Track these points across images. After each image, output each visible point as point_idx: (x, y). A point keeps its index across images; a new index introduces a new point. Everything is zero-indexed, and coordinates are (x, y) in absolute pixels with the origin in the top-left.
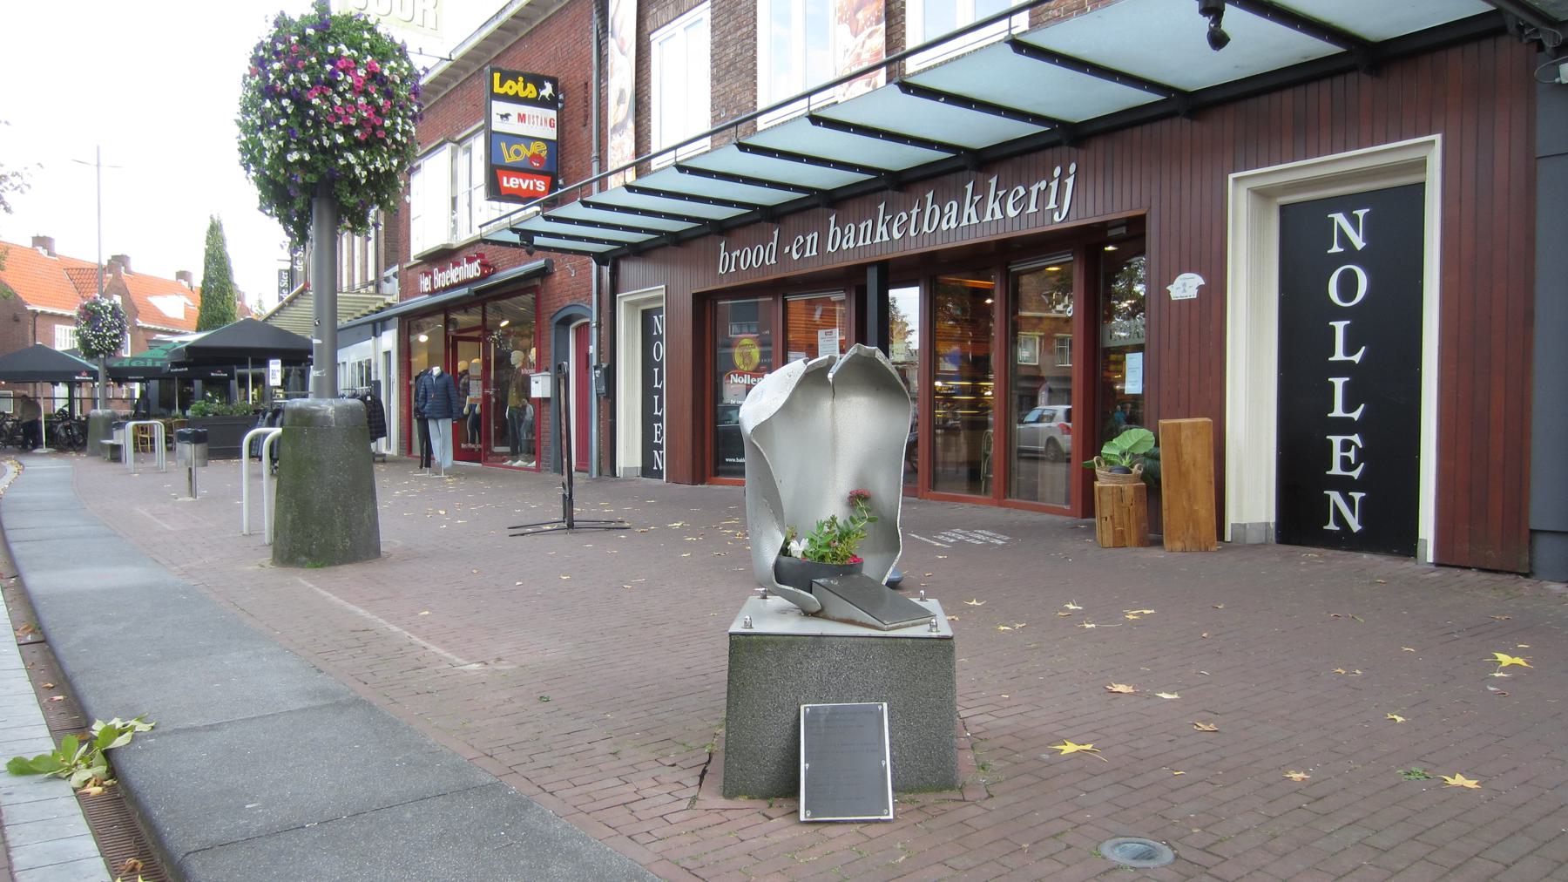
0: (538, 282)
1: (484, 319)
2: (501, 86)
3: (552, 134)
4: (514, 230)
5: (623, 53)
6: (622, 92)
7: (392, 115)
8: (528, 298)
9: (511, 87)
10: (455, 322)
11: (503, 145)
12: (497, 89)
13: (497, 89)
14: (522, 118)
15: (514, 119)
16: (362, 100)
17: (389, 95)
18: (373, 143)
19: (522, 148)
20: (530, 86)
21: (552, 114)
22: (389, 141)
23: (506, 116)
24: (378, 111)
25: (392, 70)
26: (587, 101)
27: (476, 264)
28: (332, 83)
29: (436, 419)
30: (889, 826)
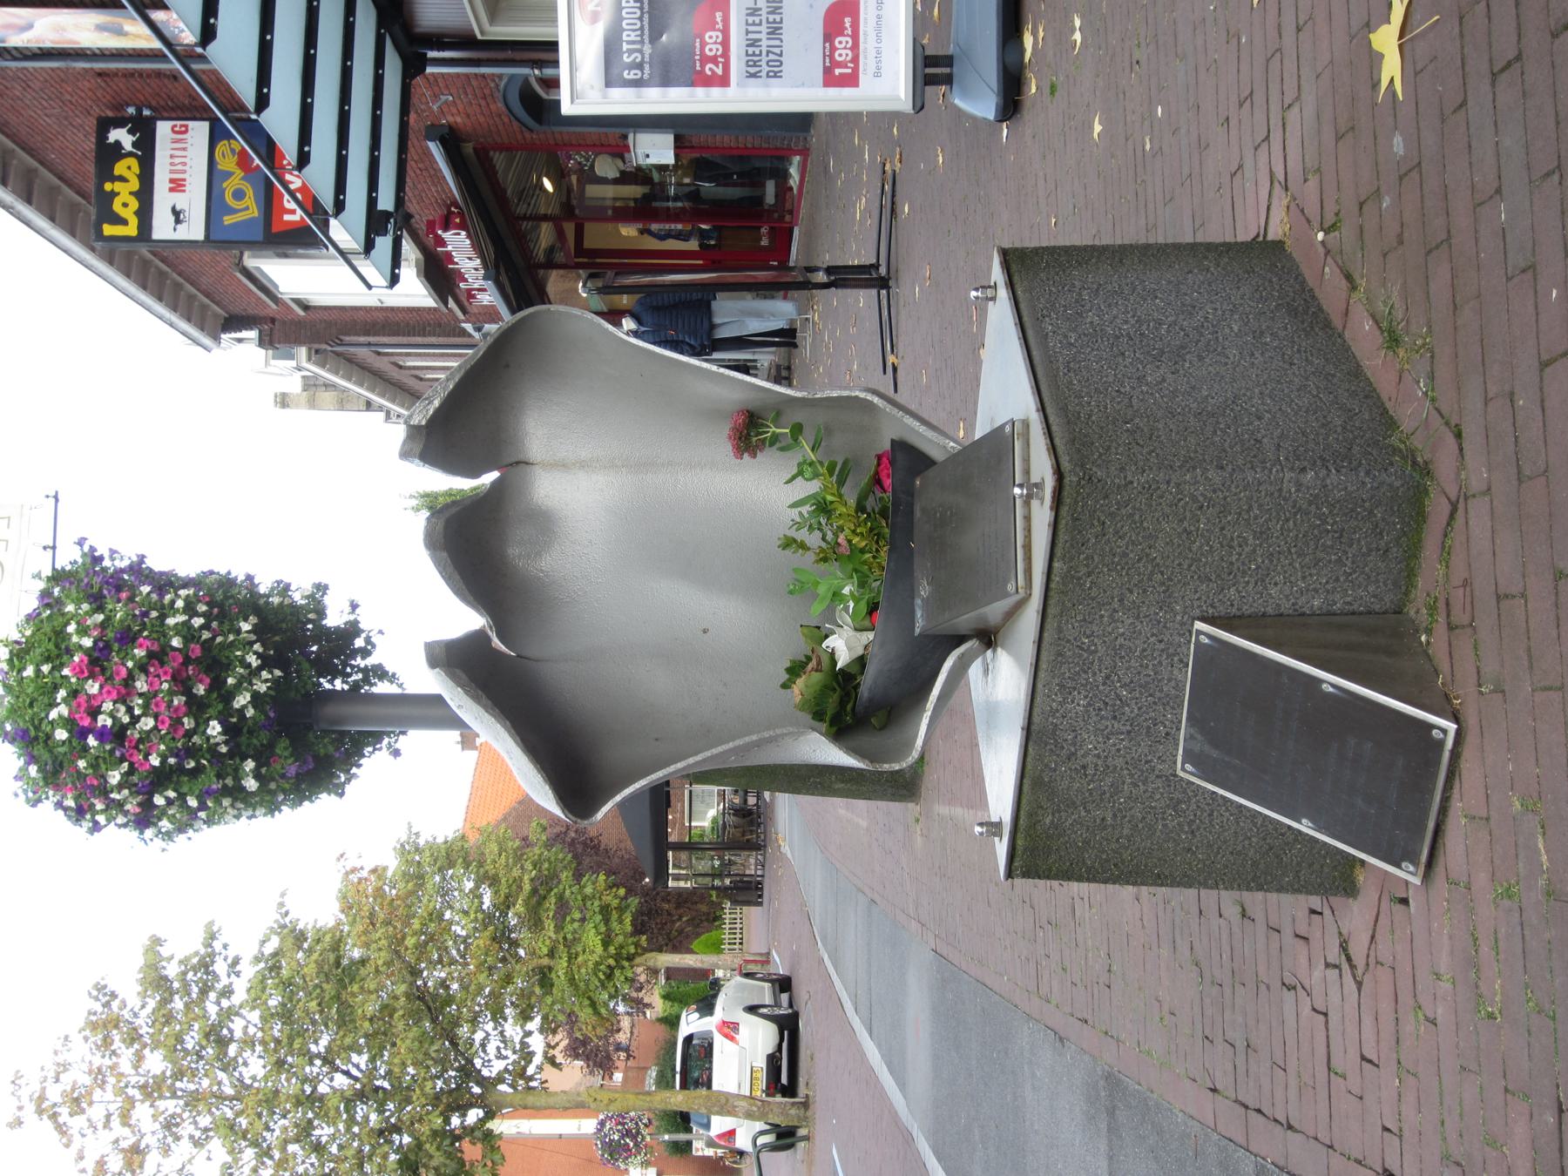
0: (468, 148)
1: (545, 218)
2: (125, 222)
3: (199, 131)
4: (369, 246)
5: (30, 27)
6: (101, 28)
7: (161, 631)
8: (499, 159)
9: (125, 202)
10: (551, 250)
11: (228, 220)
12: (131, 230)
13: (131, 230)
14: (177, 186)
15: (180, 200)
16: (141, 685)
17: (127, 638)
18: (214, 663)
19: (229, 186)
20: (120, 168)
21: (163, 128)
22: (206, 635)
23: (176, 213)
24: (158, 656)
25: (83, 631)
26: (130, 74)
27: (447, 236)
28: (118, 734)
29: (713, 327)
30: (1471, 740)
